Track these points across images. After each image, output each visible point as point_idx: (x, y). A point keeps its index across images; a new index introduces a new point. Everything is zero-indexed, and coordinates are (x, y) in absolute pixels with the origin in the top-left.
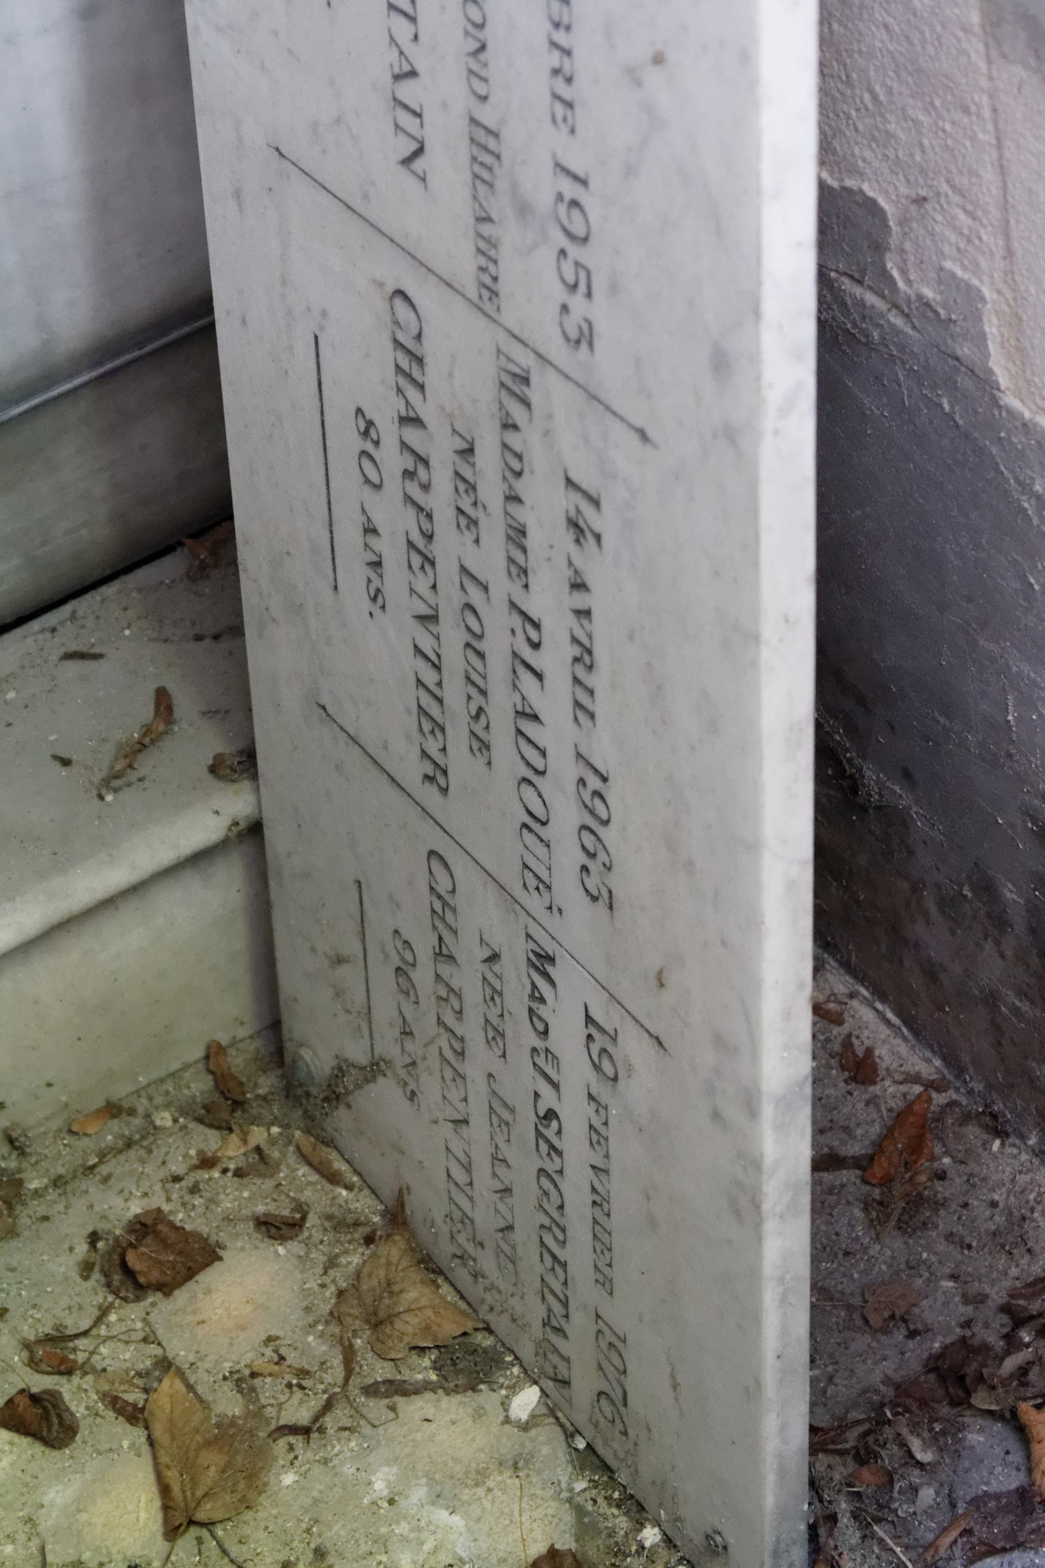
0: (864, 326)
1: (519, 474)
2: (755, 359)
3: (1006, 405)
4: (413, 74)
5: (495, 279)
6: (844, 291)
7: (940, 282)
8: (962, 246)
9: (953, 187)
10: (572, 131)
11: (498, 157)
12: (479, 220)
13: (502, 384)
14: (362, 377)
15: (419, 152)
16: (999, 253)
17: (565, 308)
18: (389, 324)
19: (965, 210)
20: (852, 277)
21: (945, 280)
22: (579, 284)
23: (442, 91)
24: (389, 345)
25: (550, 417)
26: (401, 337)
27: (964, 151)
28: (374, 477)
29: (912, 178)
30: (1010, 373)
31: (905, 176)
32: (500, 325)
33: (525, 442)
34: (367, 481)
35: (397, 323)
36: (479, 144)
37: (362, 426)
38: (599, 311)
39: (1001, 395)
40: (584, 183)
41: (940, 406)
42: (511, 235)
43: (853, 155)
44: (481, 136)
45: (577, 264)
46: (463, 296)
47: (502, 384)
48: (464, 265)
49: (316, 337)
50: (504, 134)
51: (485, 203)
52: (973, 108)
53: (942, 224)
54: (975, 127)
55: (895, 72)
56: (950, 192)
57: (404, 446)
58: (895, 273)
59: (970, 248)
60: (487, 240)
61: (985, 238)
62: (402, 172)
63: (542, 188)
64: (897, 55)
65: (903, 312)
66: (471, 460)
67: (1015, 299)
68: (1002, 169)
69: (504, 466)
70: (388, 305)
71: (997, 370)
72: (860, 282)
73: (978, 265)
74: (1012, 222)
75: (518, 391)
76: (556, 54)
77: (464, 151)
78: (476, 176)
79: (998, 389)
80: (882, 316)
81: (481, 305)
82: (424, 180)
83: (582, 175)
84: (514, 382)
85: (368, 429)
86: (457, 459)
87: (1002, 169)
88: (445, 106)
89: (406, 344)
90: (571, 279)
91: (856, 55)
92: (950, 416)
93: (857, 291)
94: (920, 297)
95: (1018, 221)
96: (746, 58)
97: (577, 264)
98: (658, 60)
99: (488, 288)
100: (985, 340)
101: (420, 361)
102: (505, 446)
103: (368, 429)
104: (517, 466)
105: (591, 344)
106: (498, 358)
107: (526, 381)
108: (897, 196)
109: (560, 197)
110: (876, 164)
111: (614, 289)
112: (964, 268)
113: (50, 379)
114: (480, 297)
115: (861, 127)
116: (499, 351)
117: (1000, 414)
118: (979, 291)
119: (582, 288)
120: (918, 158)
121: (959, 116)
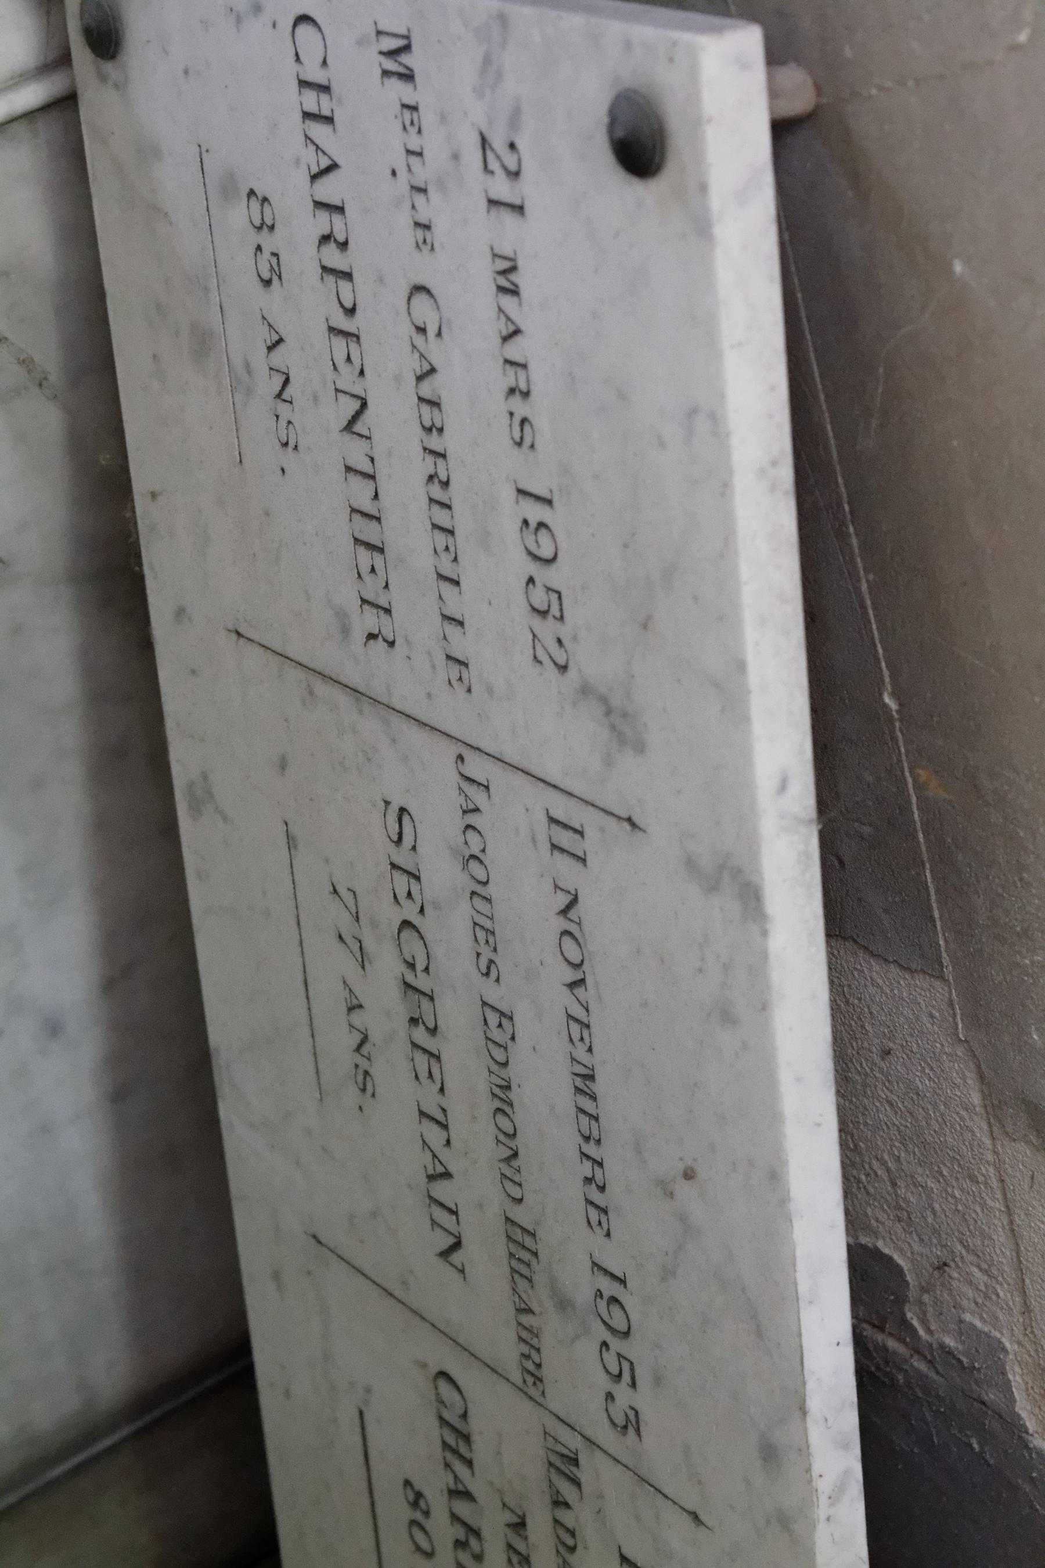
0: (888, 1369)
1: (572, 1549)
2: (804, 1451)
3: (1035, 1447)
4: (447, 1175)
5: (539, 1366)
6: (866, 1337)
7: (961, 1333)
8: (980, 1301)
9: (967, 1248)
10: (608, 1234)
11: (535, 1254)
12: (519, 1311)
13: (551, 1464)
14: (408, 1447)
15: (457, 1245)
16: (1017, 1309)
17: (610, 1396)
18: (435, 1404)
19: (981, 1270)
20: (874, 1326)
21: (964, 1330)
22: (625, 1373)
23: (477, 1190)
24: (436, 1423)
25: (601, 1496)
26: (446, 1415)
27: (974, 1215)
28: (425, 1545)
29: (926, 1238)
30: (1037, 1419)
31: (919, 1236)
32: (546, 1409)
33: (577, 1519)
34: (418, 1548)
35: (442, 1402)
36: (515, 1241)
37: (411, 1497)
38: (644, 1399)
39: (1030, 1438)
40: (623, 1282)
41: (970, 1446)
42: (552, 1327)
43: (866, 1215)
44: (518, 1235)
45: (619, 1355)
46: (508, 1380)
47: (551, 1464)
48: (506, 1350)
49: (361, 1413)
50: (540, 1234)
51: (523, 1295)
52: (981, 1179)
53: (959, 1281)
54: (984, 1195)
55: (901, 1143)
56: (964, 1252)
57: (455, 1518)
58: (915, 1323)
59: (988, 1303)
60: (529, 1330)
61: (1001, 1294)
62: (440, 1263)
63: (582, 1286)
64: (902, 1128)
65: (926, 1358)
66: (521, 1532)
67: (1036, 1351)
68: (1013, 1232)
69: (557, 1541)
70: (432, 1385)
71: (1024, 1414)
72: (881, 1329)
73: (997, 1318)
74: (1027, 1281)
75: (567, 1472)
76: (588, 1164)
77: (501, 1248)
78: (513, 1271)
79: (1027, 1432)
80: (906, 1361)
81: (526, 1390)
82: (462, 1271)
83: (620, 1275)
84: (563, 1462)
85: (417, 1499)
86: (509, 1532)
87: (1013, 1232)
88: (481, 1206)
89: (452, 1422)
90: (614, 1369)
91: (862, 1127)
92: (980, 1455)
93: (880, 1337)
94: (942, 1346)
95: (1032, 1281)
96: (775, 1176)
97: (619, 1355)
98: (689, 1175)
99: (532, 1375)
100: (1010, 1388)
101: (467, 1438)
102: (556, 1521)
103: (417, 1499)
104: (570, 1542)
105: (638, 1431)
106: (545, 1439)
107: (575, 1462)
108: (912, 1253)
109: (599, 1294)
110: (889, 1223)
111: (658, 1381)
112: (984, 1321)
113: (90, 1436)
114: (525, 1381)
115: (872, 1190)
116: (545, 1433)
117: (1030, 1455)
118: (1000, 1342)
119: (626, 1377)
120: (930, 1220)
121: (966, 1184)
